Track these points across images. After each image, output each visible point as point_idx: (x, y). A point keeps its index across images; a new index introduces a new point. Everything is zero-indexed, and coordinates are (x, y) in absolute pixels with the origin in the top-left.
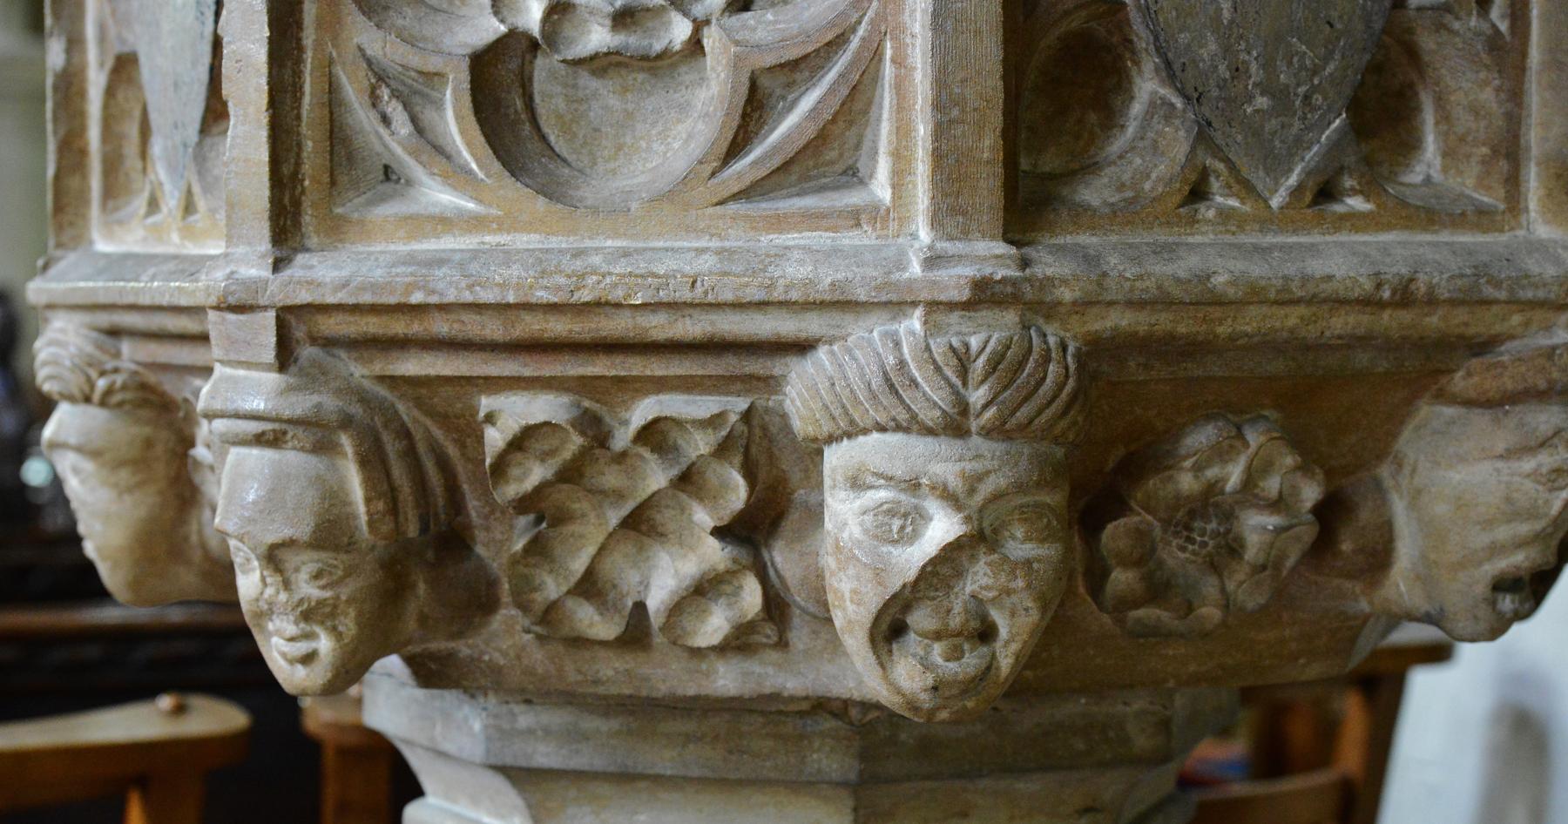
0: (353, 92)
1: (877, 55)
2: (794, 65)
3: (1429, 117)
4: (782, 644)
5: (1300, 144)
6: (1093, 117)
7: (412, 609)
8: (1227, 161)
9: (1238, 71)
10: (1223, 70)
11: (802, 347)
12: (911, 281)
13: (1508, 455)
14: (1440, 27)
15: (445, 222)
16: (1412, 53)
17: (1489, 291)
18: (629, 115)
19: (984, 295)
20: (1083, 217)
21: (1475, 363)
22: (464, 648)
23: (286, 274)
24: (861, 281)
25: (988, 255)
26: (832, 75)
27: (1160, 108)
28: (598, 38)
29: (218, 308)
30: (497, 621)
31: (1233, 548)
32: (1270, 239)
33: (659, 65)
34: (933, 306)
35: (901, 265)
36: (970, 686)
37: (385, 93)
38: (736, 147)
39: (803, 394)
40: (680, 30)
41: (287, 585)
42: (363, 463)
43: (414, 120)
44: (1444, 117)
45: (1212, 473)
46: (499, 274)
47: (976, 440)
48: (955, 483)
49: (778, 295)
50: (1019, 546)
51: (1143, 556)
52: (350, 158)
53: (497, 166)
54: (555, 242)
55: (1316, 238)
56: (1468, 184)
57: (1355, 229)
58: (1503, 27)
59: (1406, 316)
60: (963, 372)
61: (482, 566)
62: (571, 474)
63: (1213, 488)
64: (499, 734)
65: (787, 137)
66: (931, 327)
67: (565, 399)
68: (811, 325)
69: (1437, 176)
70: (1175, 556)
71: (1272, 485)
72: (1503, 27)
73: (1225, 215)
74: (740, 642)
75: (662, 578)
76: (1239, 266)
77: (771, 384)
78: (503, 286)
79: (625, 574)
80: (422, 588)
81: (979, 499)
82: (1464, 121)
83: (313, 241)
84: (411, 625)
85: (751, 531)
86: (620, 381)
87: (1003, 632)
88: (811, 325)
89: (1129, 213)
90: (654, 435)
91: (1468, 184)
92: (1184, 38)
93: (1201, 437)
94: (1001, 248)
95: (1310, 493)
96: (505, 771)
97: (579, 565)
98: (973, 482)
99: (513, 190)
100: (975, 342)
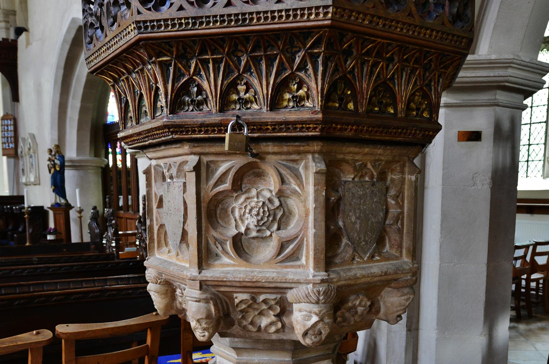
0: (211, 242)
1: (303, 240)
2: (289, 241)
3: (387, 241)
4: (284, 331)
5: (369, 249)
6: (336, 246)
7: (221, 326)
8: (358, 254)
9: (360, 238)
10: (358, 239)
11: (291, 288)
12: (310, 280)
13: (400, 296)
14: (390, 227)
15: (228, 265)
16: (385, 231)
17: (399, 272)
18: (259, 246)
19: (323, 281)
20: (336, 265)
21: (395, 282)
22: (228, 331)
23: (201, 274)
24: (302, 278)
25: (322, 275)
26: (295, 243)
27: (346, 244)
28: (254, 234)
29: (190, 279)
30: (234, 327)
31: (356, 313)
32: (365, 265)
33: (264, 238)
34: (314, 284)
35: (308, 276)
36: (318, 342)
37: (217, 243)
38: (279, 254)
39: (290, 296)
40: (268, 233)
41: (200, 325)
42: (214, 305)
43: (222, 247)
44: (390, 241)
45: (354, 303)
46: (239, 276)
47: (320, 304)
48: (317, 312)
49: (287, 281)
50: (327, 320)
51: (343, 316)
52: (211, 253)
53: (237, 256)
54: (248, 269)
55: (371, 265)
56: (394, 252)
57: (378, 262)
58: (400, 227)
59: (386, 277)
60: (319, 294)
61: (232, 319)
62: (249, 306)
63: (355, 305)
64: (231, 342)
65: (288, 253)
66: (314, 287)
67: (249, 295)
68: (293, 285)
69: (389, 251)
70: (347, 315)
71: (363, 303)
72: (400, 227)
73: (358, 262)
74: (277, 331)
75: (264, 322)
76: (361, 272)
77: (285, 293)
78: (240, 278)
79: (257, 321)
80: (222, 323)
81: (321, 314)
82: (393, 242)
83: (205, 268)
84: (220, 329)
85: (279, 316)
86: (259, 292)
87: (323, 333)
88: (293, 285)
89: (343, 263)
90: (265, 301)
91: (394, 252)
92: (352, 234)
93: (352, 297)
94: (325, 273)
95: (369, 303)
96: (233, 348)
97: (250, 320)
98: (320, 311)
99: (240, 260)
100: (321, 289)
